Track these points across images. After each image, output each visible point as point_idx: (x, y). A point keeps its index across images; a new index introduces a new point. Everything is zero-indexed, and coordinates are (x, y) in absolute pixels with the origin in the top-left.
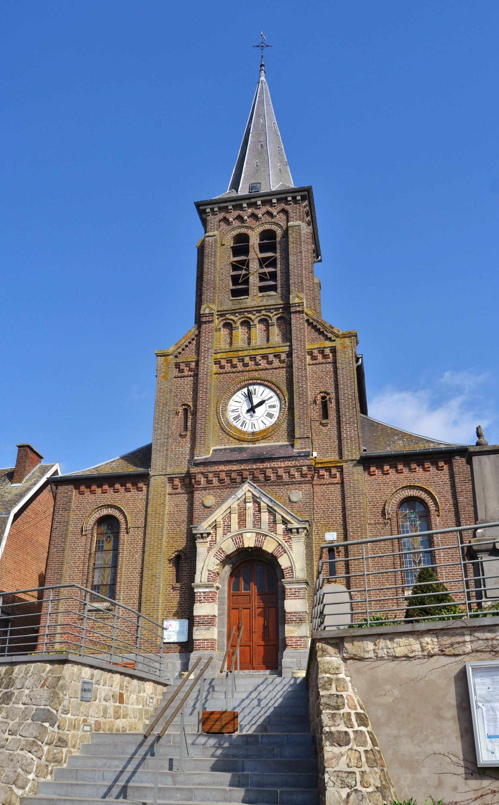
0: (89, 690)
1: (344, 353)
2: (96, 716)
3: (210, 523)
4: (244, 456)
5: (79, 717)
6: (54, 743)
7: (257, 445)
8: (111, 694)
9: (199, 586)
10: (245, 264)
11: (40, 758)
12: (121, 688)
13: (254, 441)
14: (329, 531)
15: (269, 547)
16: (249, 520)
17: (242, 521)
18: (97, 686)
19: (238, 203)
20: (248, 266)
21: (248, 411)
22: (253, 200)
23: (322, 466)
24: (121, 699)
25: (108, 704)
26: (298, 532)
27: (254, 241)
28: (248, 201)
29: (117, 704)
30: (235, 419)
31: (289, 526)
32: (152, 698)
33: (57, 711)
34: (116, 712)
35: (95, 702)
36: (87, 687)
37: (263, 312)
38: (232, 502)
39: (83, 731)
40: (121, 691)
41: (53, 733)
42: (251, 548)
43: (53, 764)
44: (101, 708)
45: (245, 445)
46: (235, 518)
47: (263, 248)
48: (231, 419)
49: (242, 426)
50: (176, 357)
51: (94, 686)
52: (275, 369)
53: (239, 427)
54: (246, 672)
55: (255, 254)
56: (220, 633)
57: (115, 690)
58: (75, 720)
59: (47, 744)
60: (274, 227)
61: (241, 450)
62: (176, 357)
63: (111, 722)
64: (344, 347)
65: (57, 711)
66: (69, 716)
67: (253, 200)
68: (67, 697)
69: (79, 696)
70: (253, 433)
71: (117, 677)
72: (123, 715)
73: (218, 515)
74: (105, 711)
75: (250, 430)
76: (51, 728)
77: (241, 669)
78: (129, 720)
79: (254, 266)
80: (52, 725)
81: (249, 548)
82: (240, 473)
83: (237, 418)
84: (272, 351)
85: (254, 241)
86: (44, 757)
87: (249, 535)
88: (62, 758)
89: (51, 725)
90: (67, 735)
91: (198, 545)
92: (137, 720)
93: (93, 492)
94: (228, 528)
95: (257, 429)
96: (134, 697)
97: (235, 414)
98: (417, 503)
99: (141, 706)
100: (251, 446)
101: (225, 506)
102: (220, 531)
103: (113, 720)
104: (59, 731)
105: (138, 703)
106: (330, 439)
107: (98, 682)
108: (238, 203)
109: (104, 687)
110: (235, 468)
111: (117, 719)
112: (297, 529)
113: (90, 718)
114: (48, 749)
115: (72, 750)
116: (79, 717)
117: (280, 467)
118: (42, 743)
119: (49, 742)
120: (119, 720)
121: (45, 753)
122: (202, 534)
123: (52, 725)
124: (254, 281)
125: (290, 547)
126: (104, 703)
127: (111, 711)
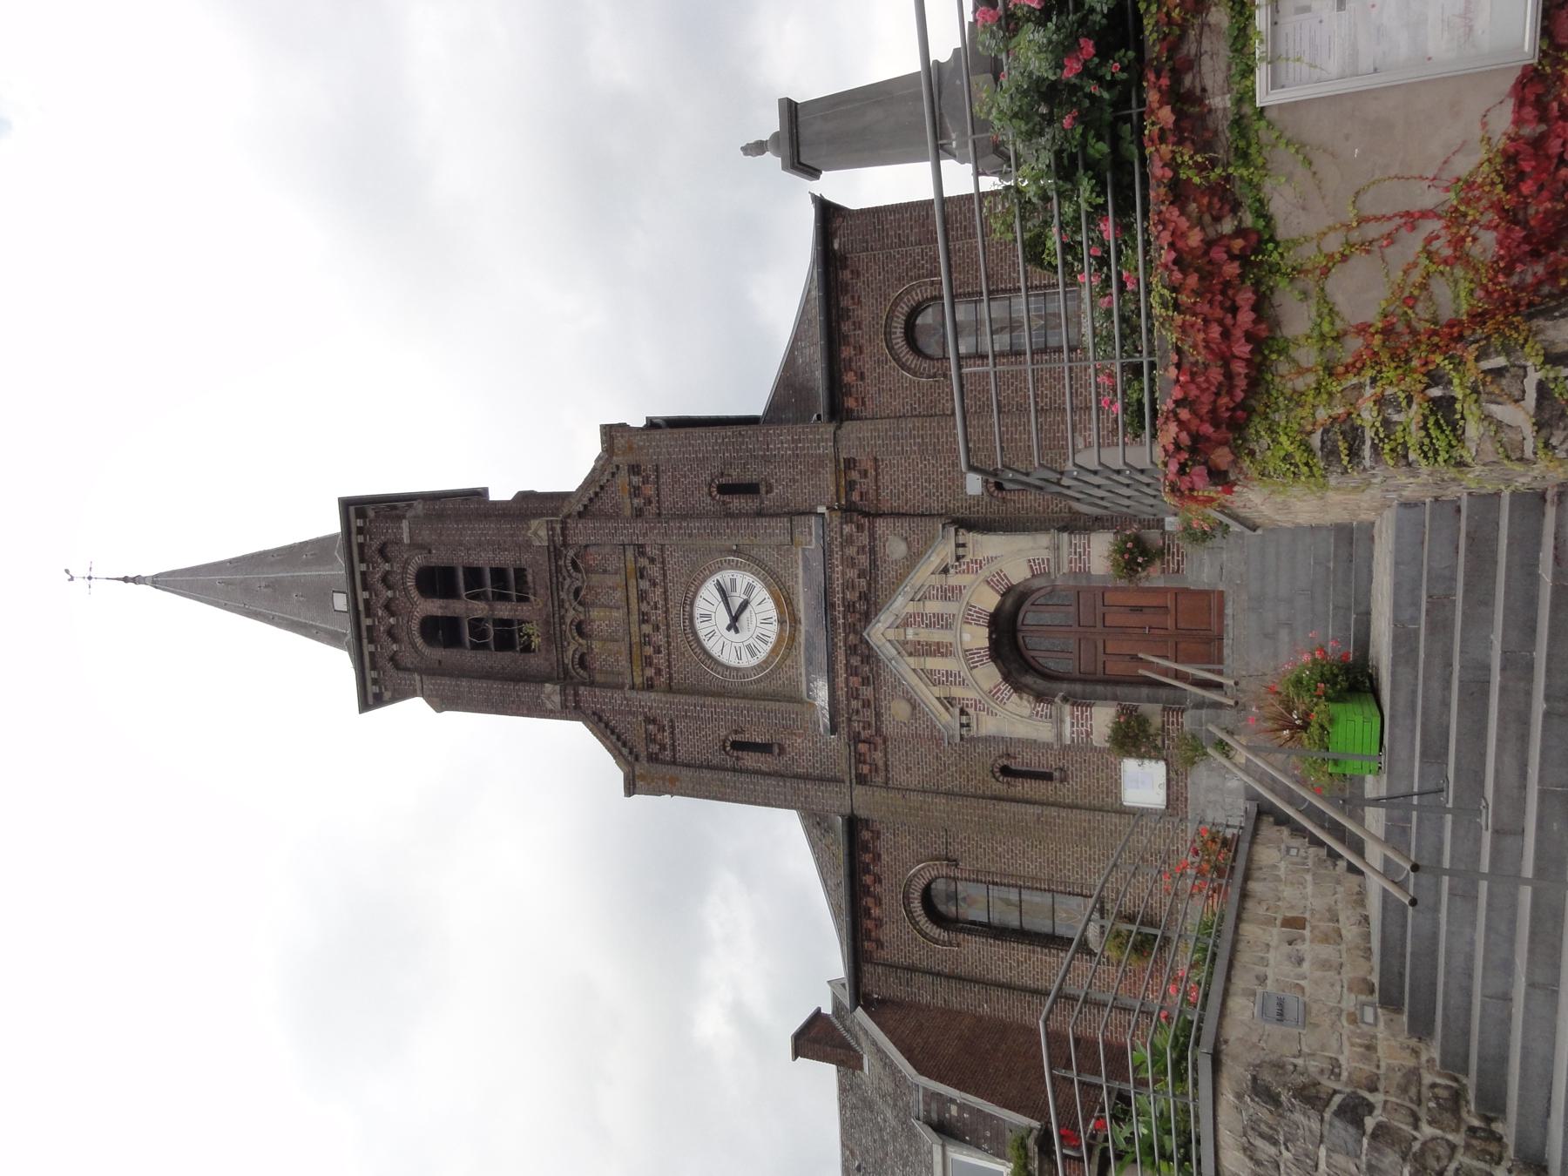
0: (1281, 1003)
1: (640, 448)
2: (1338, 989)
3: (942, 710)
4: (821, 641)
5: (1345, 1033)
6: (1414, 1107)
7: (802, 615)
8: (1286, 948)
9: (1059, 736)
10: (477, 625)
11: (1453, 1148)
12: (1270, 922)
13: (795, 621)
14: (963, 487)
15: (990, 601)
16: (937, 636)
17: (938, 650)
18: (1269, 982)
19: (364, 634)
20: (480, 620)
21: (729, 628)
22: (361, 607)
23: (843, 495)
24: (1295, 923)
25: (1308, 957)
26: (964, 545)
27: (433, 607)
28: (363, 616)
29: (1307, 933)
30: (753, 654)
31: (951, 560)
32: (1288, 849)
33: (1335, 1092)
34: (1326, 939)
35: (1307, 990)
36: (1273, 1009)
37: (563, 595)
38: (906, 668)
39: (1375, 1024)
40: (1278, 922)
41: (1389, 1106)
42: (991, 633)
43: (1464, 1115)
44: (1318, 974)
45: (802, 639)
46: (932, 663)
47: (450, 592)
48: (754, 662)
49: (766, 643)
50: (637, 759)
51: (1269, 989)
52: (665, 575)
53: (769, 648)
54: (1226, 651)
55: (465, 608)
56: (1150, 700)
57: (1276, 938)
58: (1352, 1045)
59: (1416, 1127)
60: (412, 570)
61: (810, 645)
62: (637, 759)
63: (1348, 950)
64: (631, 448)
65: (1335, 1092)
66: (1343, 1060)
67: (361, 607)
68: (1300, 1062)
69: (1296, 1031)
70: (781, 622)
71: (1248, 929)
72: (1331, 920)
73: (929, 696)
74: (1325, 965)
75: (775, 627)
76: (1377, 1112)
77: (1220, 661)
78: (1340, 906)
79: (480, 609)
80: (1370, 1108)
81: (990, 638)
82: (852, 650)
83: (752, 651)
84: (632, 582)
85: (433, 607)
86: (1450, 1137)
87: (966, 637)
88: (1447, 1087)
89: (1370, 1113)
90: (1390, 1068)
91: (983, 732)
92: (1340, 889)
93: (879, 923)
94: (950, 678)
95: (774, 614)
96: (1288, 892)
97: (745, 654)
98: (919, 321)
99: (1309, 877)
100: (803, 628)
101: (913, 680)
102: (957, 692)
103: (1343, 947)
104: (1381, 1088)
105: (1302, 884)
106: (794, 481)
107: (1262, 980)
108: (364, 634)
109: (1272, 962)
110: (841, 658)
111: (1340, 936)
112: (958, 546)
113: (1344, 1005)
114: (1430, 1123)
115: (1424, 1058)
116: (1345, 1033)
117: (843, 573)
118: (1415, 1139)
119: (1411, 1120)
120: (1344, 932)
121: (1439, 1132)
122: (962, 725)
123: (1370, 1108)
124: (504, 611)
125: (991, 560)
126: (1306, 965)
127: (1327, 951)
